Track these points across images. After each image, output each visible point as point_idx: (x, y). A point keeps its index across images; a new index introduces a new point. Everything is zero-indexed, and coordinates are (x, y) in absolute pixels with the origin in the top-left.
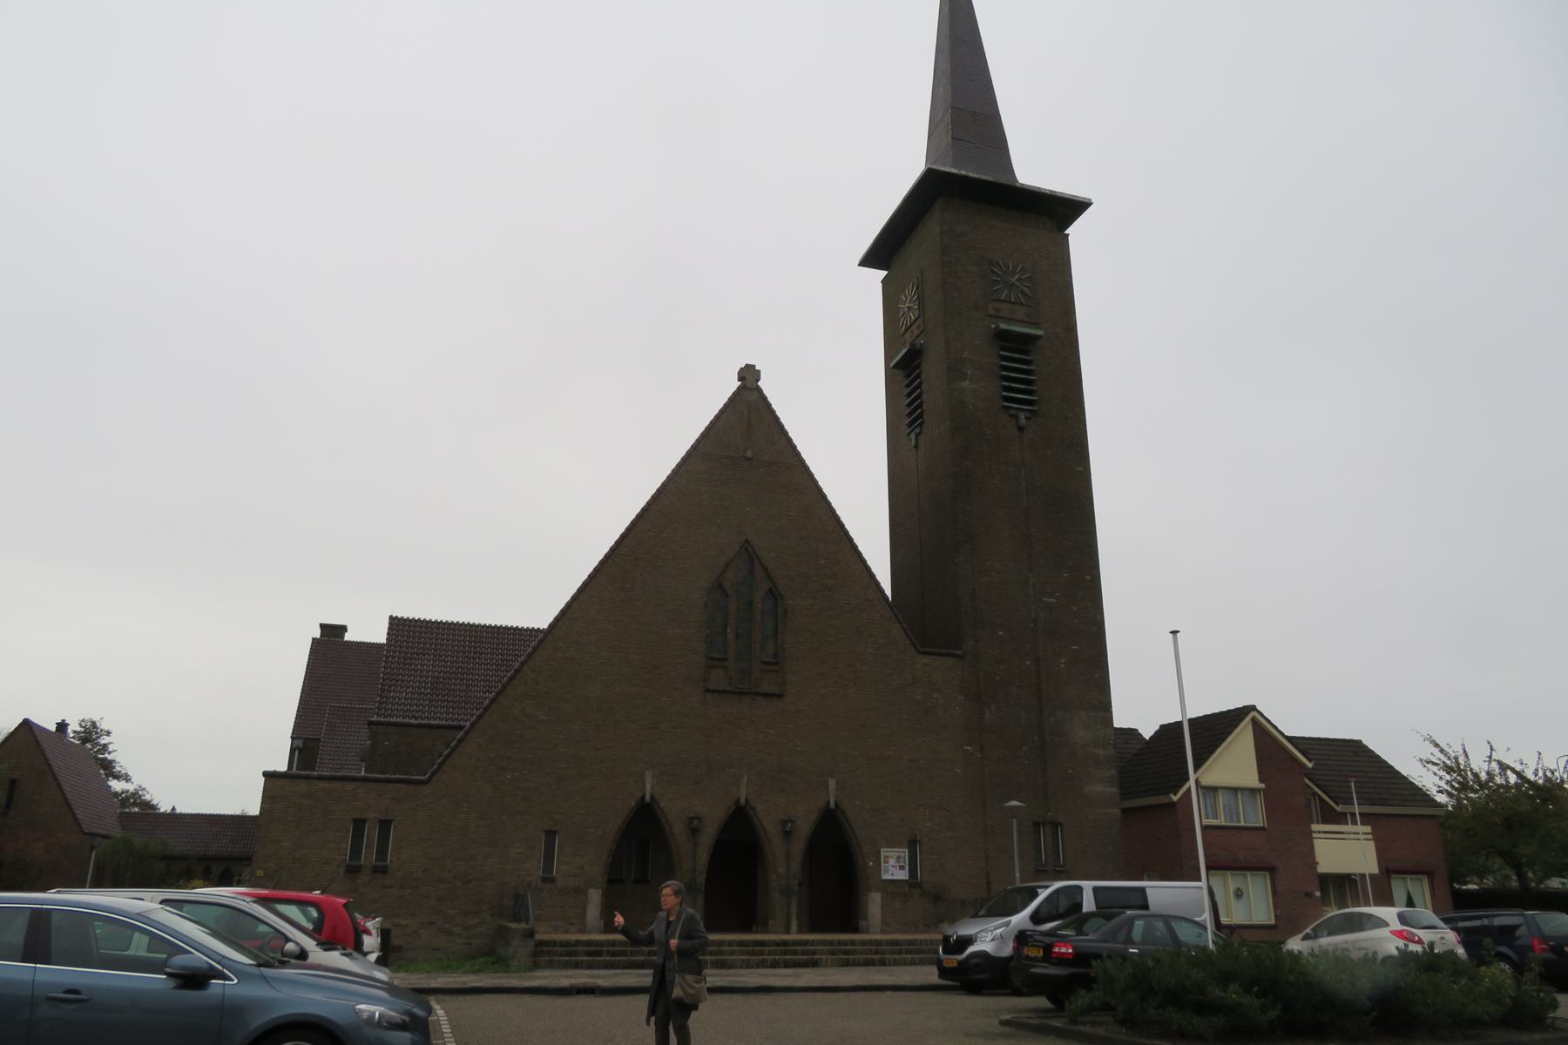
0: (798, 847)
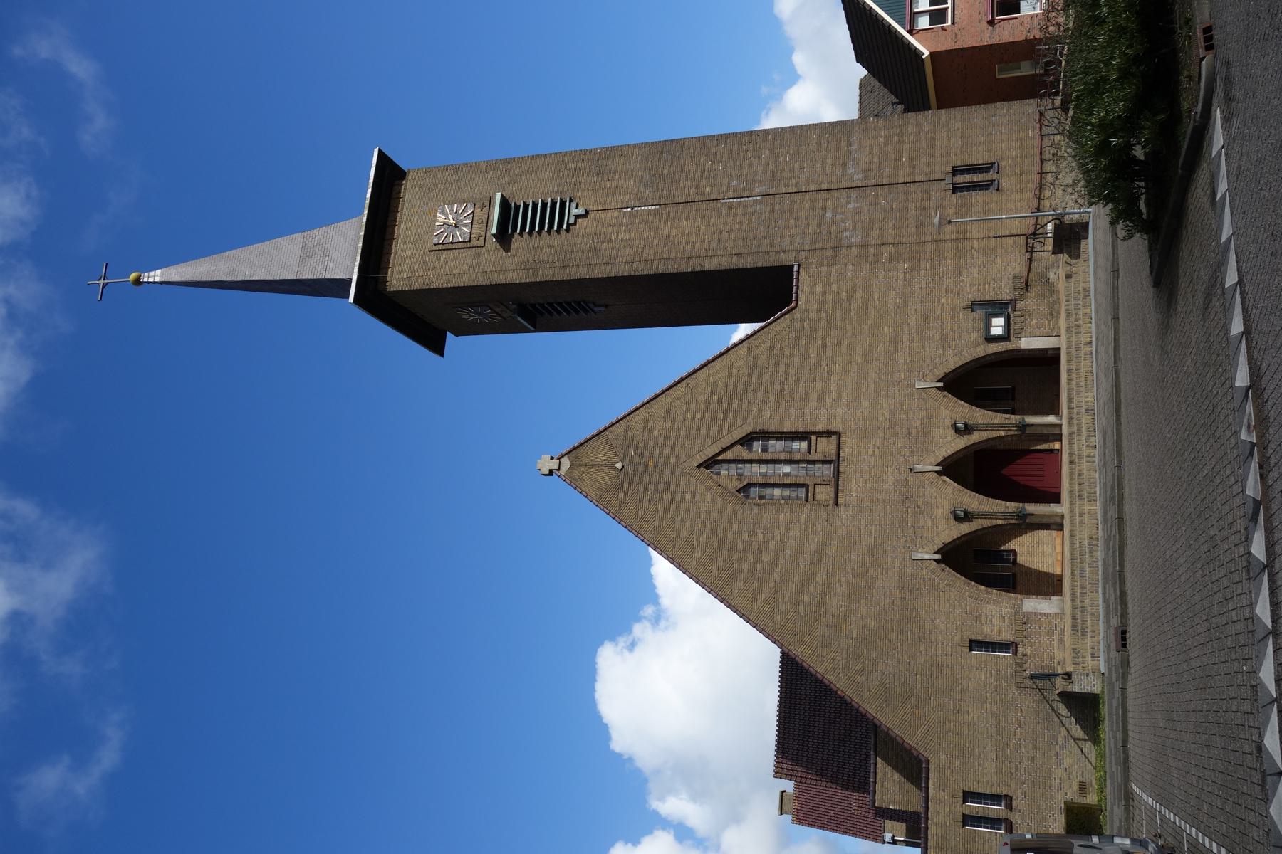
0: (980, 416)
